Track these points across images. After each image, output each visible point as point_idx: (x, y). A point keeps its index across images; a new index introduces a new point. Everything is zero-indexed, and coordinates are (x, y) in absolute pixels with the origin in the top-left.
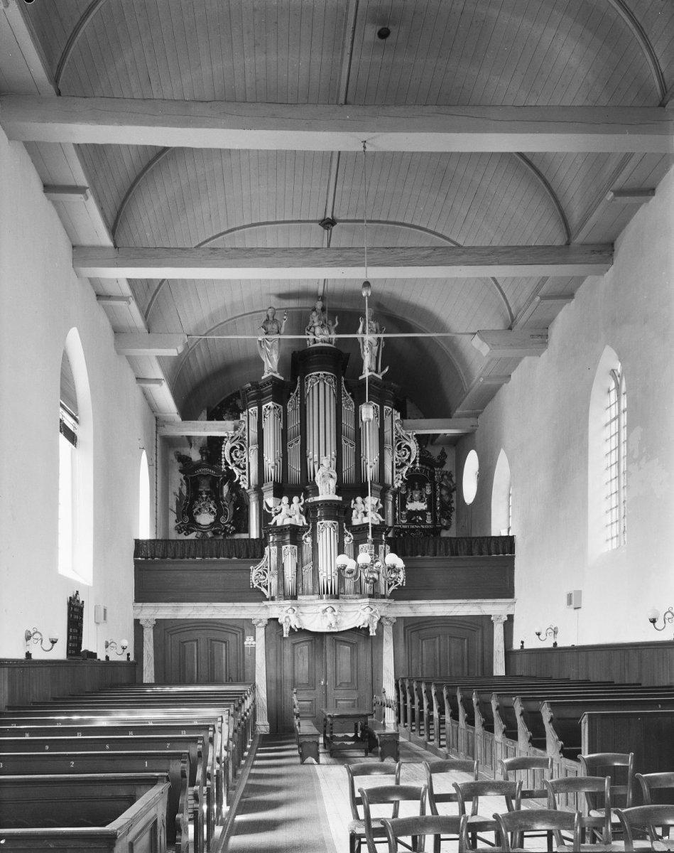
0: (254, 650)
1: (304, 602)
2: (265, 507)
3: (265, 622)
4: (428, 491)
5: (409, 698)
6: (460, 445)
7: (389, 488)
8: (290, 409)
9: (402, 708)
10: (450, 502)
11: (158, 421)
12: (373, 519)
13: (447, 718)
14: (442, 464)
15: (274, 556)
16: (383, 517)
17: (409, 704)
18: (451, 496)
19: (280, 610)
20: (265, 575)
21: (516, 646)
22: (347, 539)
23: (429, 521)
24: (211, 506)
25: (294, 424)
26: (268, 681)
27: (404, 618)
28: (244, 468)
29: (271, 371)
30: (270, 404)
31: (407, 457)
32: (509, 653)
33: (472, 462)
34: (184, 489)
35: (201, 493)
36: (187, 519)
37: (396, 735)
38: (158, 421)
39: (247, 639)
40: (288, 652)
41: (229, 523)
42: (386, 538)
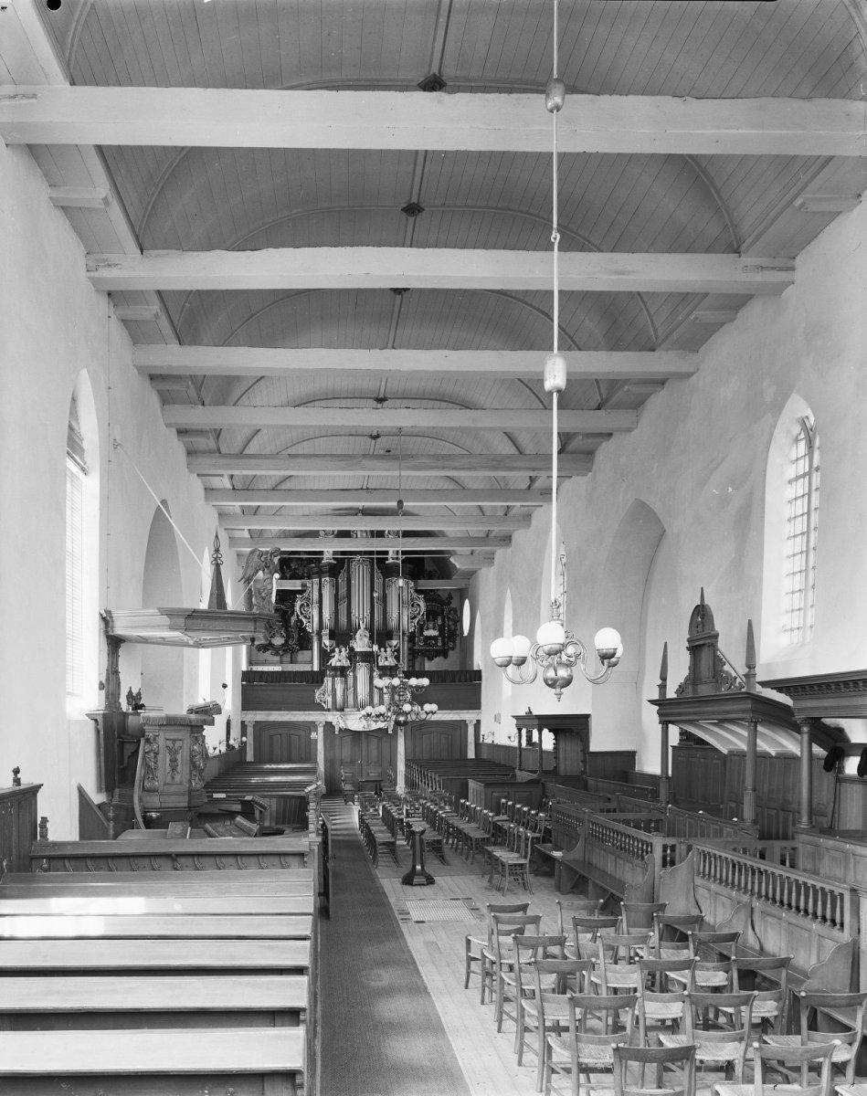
4: (440, 622)
6: (463, 593)
14: (449, 603)
15: (330, 684)
22: (375, 674)
23: (440, 644)
25: (343, 591)
26: (326, 760)
30: (327, 579)
32: (477, 745)
40: (338, 742)
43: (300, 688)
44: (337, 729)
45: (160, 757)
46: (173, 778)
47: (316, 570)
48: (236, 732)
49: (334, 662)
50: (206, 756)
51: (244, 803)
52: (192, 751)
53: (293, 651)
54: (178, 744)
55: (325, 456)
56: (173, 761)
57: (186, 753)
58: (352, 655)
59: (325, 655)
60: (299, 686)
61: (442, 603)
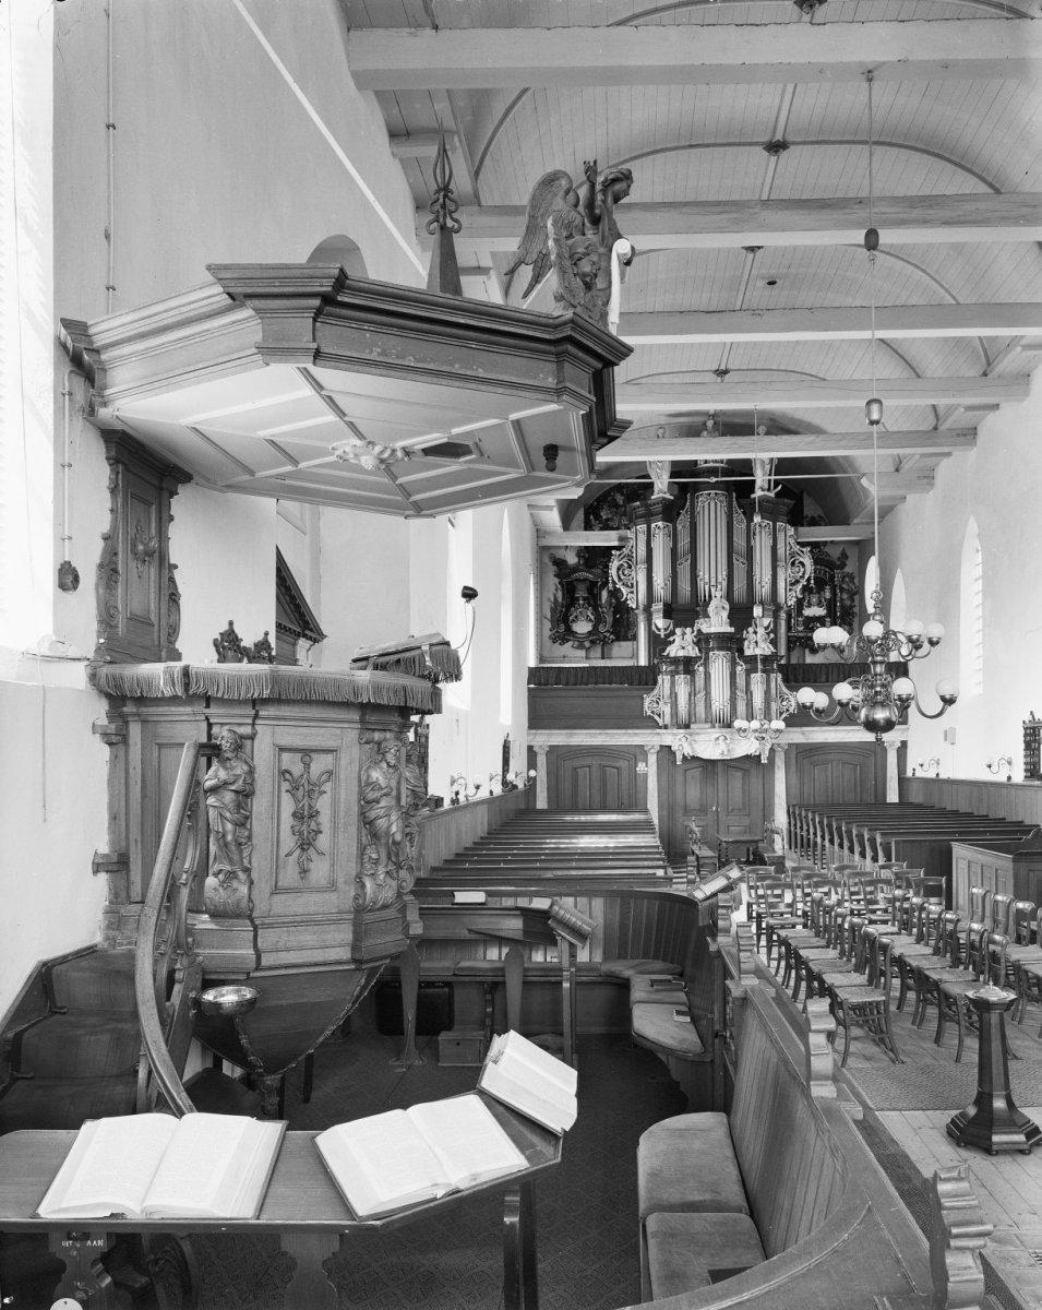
0: (646, 776)
1: (698, 731)
2: (654, 628)
3: (658, 748)
4: (828, 595)
5: (799, 825)
6: (863, 548)
7: (781, 608)
8: (679, 527)
9: (793, 834)
10: (852, 607)
11: (540, 532)
12: (764, 649)
13: (827, 843)
14: (843, 565)
15: (667, 685)
16: (775, 648)
17: (798, 830)
18: (853, 600)
19: (675, 739)
20: (658, 703)
21: (909, 774)
22: (739, 668)
24: (589, 614)
25: (684, 542)
27: (797, 745)
28: (632, 587)
29: (660, 491)
30: (660, 524)
31: (800, 574)
32: (902, 780)
33: (873, 566)
34: (560, 594)
35: (577, 599)
36: (562, 627)
37: (783, 858)
38: (540, 532)
39: (640, 765)
40: (680, 778)
41: (608, 631)
42: (779, 666)
43: (620, 693)
44: (679, 758)
45: (260, 805)
46: (304, 872)
47: (641, 511)
48: (518, 762)
49: (673, 651)
50: (421, 802)
51: (527, 914)
52: (365, 785)
53: (605, 643)
54: (320, 764)
55: (686, 204)
56: (305, 816)
57: (348, 794)
58: (702, 640)
59: (658, 643)
60: (618, 690)
61: (831, 565)
